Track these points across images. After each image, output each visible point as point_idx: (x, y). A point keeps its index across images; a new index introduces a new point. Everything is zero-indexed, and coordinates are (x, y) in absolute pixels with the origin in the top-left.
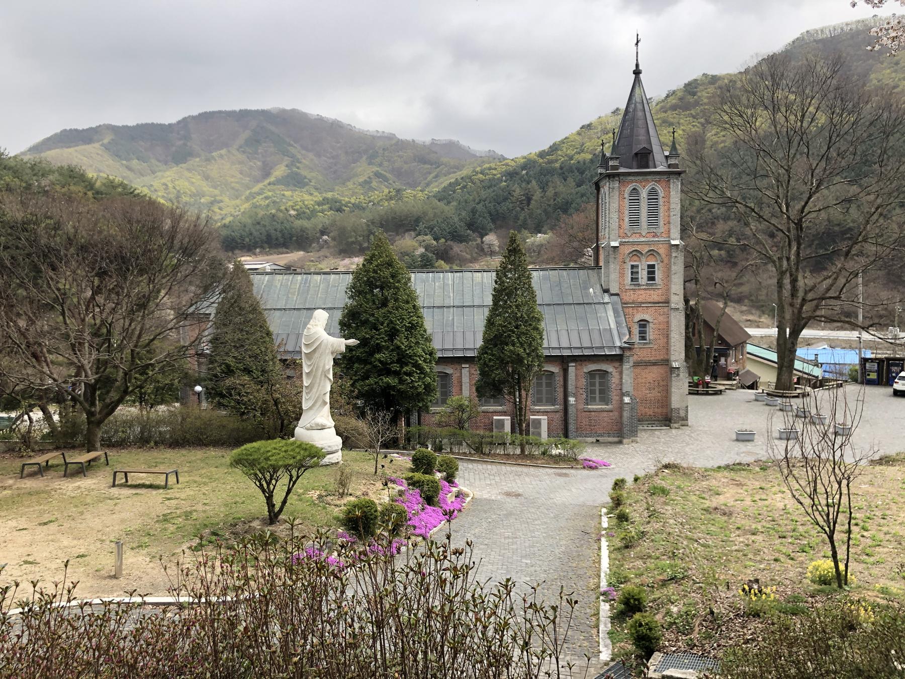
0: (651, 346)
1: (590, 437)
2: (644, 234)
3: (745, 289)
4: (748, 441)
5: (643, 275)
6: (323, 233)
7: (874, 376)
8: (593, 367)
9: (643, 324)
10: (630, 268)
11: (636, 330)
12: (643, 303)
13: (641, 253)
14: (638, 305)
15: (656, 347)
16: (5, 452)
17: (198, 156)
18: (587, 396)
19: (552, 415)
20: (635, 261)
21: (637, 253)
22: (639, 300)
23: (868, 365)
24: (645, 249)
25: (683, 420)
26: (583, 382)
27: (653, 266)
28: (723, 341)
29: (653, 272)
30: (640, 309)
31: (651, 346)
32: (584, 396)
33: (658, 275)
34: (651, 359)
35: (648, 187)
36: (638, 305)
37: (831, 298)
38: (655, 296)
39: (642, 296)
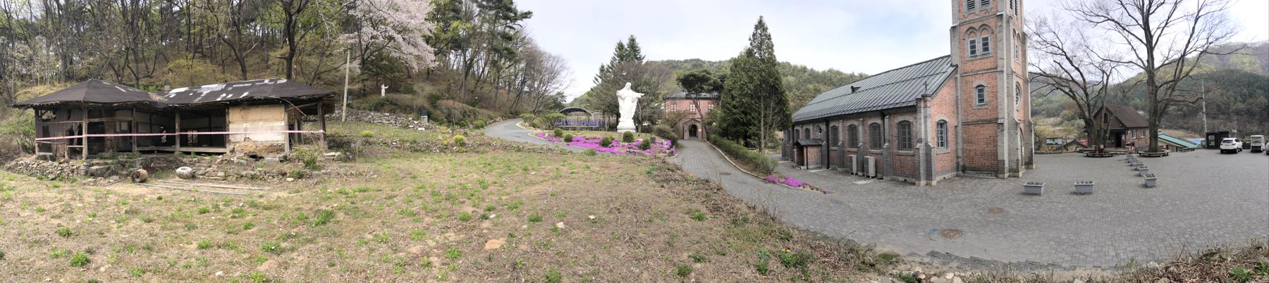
0: (986, 107)
1: (901, 176)
2: (977, 13)
5: (979, 47)
7: (1213, 144)
8: (901, 118)
9: (980, 88)
10: (969, 43)
11: (975, 94)
12: (979, 71)
13: (975, 29)
14: (975, 73)
15: (990, 108)
16: (438, 5)
17: (64, 216)
18: (899, 142)
19: (879, 157)
20: (973, 37)
21: (971, 30)
22: (977, 69)
23: (1210, 137)
24: (977, 25)
25: (1015, 171)
26: (895, 131)
27: (987, 39)
28: (1123, 125)
29: (987, 44)
30: (977, 76)
31: (986, 107)
32: (897, 142)
33: (990, 46)
34: (988, 118)
35: (805, 127)
36: (975, 73)
37: (1183, 77)
38: (988, 63)
39: (979, 65)
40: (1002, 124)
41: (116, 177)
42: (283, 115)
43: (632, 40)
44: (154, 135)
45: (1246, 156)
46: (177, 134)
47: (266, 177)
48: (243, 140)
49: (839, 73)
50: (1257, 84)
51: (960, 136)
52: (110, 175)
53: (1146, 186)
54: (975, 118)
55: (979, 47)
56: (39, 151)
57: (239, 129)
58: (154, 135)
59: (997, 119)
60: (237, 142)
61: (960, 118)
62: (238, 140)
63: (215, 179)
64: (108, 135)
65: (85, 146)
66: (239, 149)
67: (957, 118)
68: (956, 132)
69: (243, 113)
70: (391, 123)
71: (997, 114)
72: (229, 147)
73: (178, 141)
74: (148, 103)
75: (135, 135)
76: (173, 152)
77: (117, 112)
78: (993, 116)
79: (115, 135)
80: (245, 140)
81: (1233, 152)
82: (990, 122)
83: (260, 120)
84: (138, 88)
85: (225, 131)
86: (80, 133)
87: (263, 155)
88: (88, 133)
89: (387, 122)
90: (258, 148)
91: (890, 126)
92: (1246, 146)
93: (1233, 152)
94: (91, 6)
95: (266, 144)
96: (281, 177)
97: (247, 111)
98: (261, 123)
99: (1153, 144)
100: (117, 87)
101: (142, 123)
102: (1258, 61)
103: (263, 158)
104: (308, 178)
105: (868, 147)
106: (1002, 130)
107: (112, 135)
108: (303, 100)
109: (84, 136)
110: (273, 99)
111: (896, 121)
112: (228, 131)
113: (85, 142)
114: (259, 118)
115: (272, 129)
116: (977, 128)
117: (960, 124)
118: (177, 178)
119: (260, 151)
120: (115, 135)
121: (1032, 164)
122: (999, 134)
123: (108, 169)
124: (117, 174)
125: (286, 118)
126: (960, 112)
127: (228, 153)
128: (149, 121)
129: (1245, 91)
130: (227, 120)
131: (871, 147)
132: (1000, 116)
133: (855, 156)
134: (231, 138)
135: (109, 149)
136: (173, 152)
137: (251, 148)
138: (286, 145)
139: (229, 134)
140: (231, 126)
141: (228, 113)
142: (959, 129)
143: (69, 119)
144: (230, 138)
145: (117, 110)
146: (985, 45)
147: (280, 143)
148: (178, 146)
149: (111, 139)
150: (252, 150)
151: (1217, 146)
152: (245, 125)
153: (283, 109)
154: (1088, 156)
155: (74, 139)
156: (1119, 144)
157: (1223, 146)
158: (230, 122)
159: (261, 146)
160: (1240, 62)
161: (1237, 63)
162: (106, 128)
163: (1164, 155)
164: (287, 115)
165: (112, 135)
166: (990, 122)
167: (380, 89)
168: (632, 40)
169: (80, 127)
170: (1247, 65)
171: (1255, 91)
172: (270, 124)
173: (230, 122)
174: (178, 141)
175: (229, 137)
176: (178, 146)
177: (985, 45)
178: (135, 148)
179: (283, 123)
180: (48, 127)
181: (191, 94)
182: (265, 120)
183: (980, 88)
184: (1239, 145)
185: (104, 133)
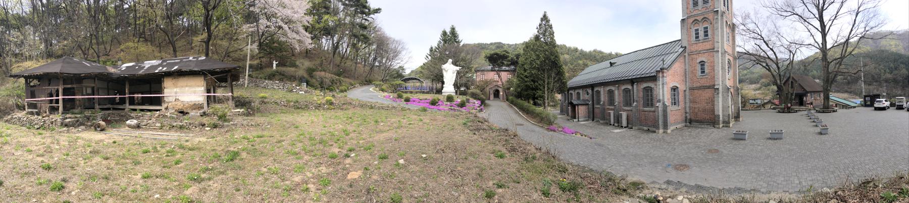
0: (707, 77)
1: (645, 126)
2: (700, 9)
3: (852, 90)
4: (742, 139)
5: (701, 34)
6: (747, 79)
7: (869, 103)
8: (645, 85)
9: (702, 63)
10: (694, 31)
11: (699, 67)
12: (701, 51)
13: (699, 21)
14: (699, 53)
15: (709, 77)
18: (644, 102)
19: (630, 112)
20: (697, 27)
21: (696, 21)
22: (700, 50)
24: (700, 18)
25: (727, 123)
26: (641, 94)
27: (707, 28)
28: (805, 90)
29: (707, 31)
30: (700, 55)
31: (707, 77)
32: (642, 102)
33: (709, 33)
34: (708, 84)
36: (699, 53)
37: (848, 55)
38: (708, 46)
39: (701, 46)
40: (718, 89)
41: (83, 127)
42: (203, 82)
43: (453, 29)
44: (110, 96)
45: (892, 112)
46: (127, 96)
47: (190, 127)
48: (174, 100)
49: (601, 52)
50: (900, 60)
51: (687, 97)
52: (79, 126)
53: (821, 134)
54: (698, 85)
55: (701, 34)
56: (28, 109)
57: (171, 93)
58: (110, 96)
59: (714, 85)
60: (170, 102)
61: (688, 85)
62: (171, 101)
63: (154, 129)
64: (77, 97)
65: (61, 105)
66: (172, 107)
67: (686, 84)
68: (685, 95)
69: (174, 81)
70: (280, 88)
71: (714, 81)
72: (164, 106)
73: (127, 101)
74: (106, 74)
75: (97, 97)
76: (124, 109)
77: (84, 80)
78: (712, 84)
79: (83, 97)
80: (175, 100)
81: (883, 109)
82: (709, 87)
83: (187, 86)
84: (99, 63)
85: (161, 94)
86: (58, 95)
87: (189, 111)
88: (63, 96)
89: (278, 88)
90: (185, 106)
91: (638, 90)
92: (892, 105)
93: (883, 109)
94: (66, 4)
95: (190, 104)
96: (201, 127)
97: (177, 80)
98: (187, 88)
99: (826, 103)
100: (83, 62)
101: (101, 88)
102: (901, 44)
103: (189, 113)
104: (220, 128)
105: (622, 105)
106: (718, 94)
107: (80, 97)
108: (217, 72)
109: (60, 97)
110: (195, 71)
111: (642, 87)
112: (164, 94)
113: (61, 102)
114: (186, 85)
115: (195, 92)
116: (700, 92)
117: (688, 89)
118: (127, 128)
119: (186, 108)
120: (83, 97)
121: (739, 118)
122: (715, 96)
123: (78, 121)
124: (84, 125)
125: (205, 85)
126: (687, 81)
127: (163, 110)
128: (106, 87)
129: (892, 65)
130: (163, 86)
131: (624, 106)
132: (716, 83)
133: (613, 112)
134: (166, 99)
135: (78, 107)
136: (124, 109)
137: (180, 106)
138: (205, 104)
139: (164, 96)
140: (165, 90)
141: (164, 81)
142: (687, 93)
143: (49, 85)
144: (165, 99)
145: (84, 79)
146: (706, 32)
147: (201, 103)
148: (127, 105)
149: (79, 100)
150: (180, 107)
151: (872, 105)
152: (175, 90)
153: (203, 78)
154: (779, 112)
155: (53, 99)
156: (801, 103)
157: (876, 105)
158: (164, 88)
159: (187, 105)
160: (888, 45)
161: (886, 45)
162: (76, 91)
163: (834, 111)
164: (205, 82)
165: (80, 97)
166: (709, 87)
167: (272, 64)
168: (453, 29)
169: (57, 91)
170: (893, 46)
171: (899, 66)
172: (194, 89)
173: (164, 88)
174: (127, 101)
175: (164, 99)
176: (127, 105)
177: (706, 32)
178: (97, 106)
179: (203, 89)
180: (34, 91)
181: (137, 67)
182: (190, 86)
183: (702, 63)
184: (887, 104)
185: (74, 96)
